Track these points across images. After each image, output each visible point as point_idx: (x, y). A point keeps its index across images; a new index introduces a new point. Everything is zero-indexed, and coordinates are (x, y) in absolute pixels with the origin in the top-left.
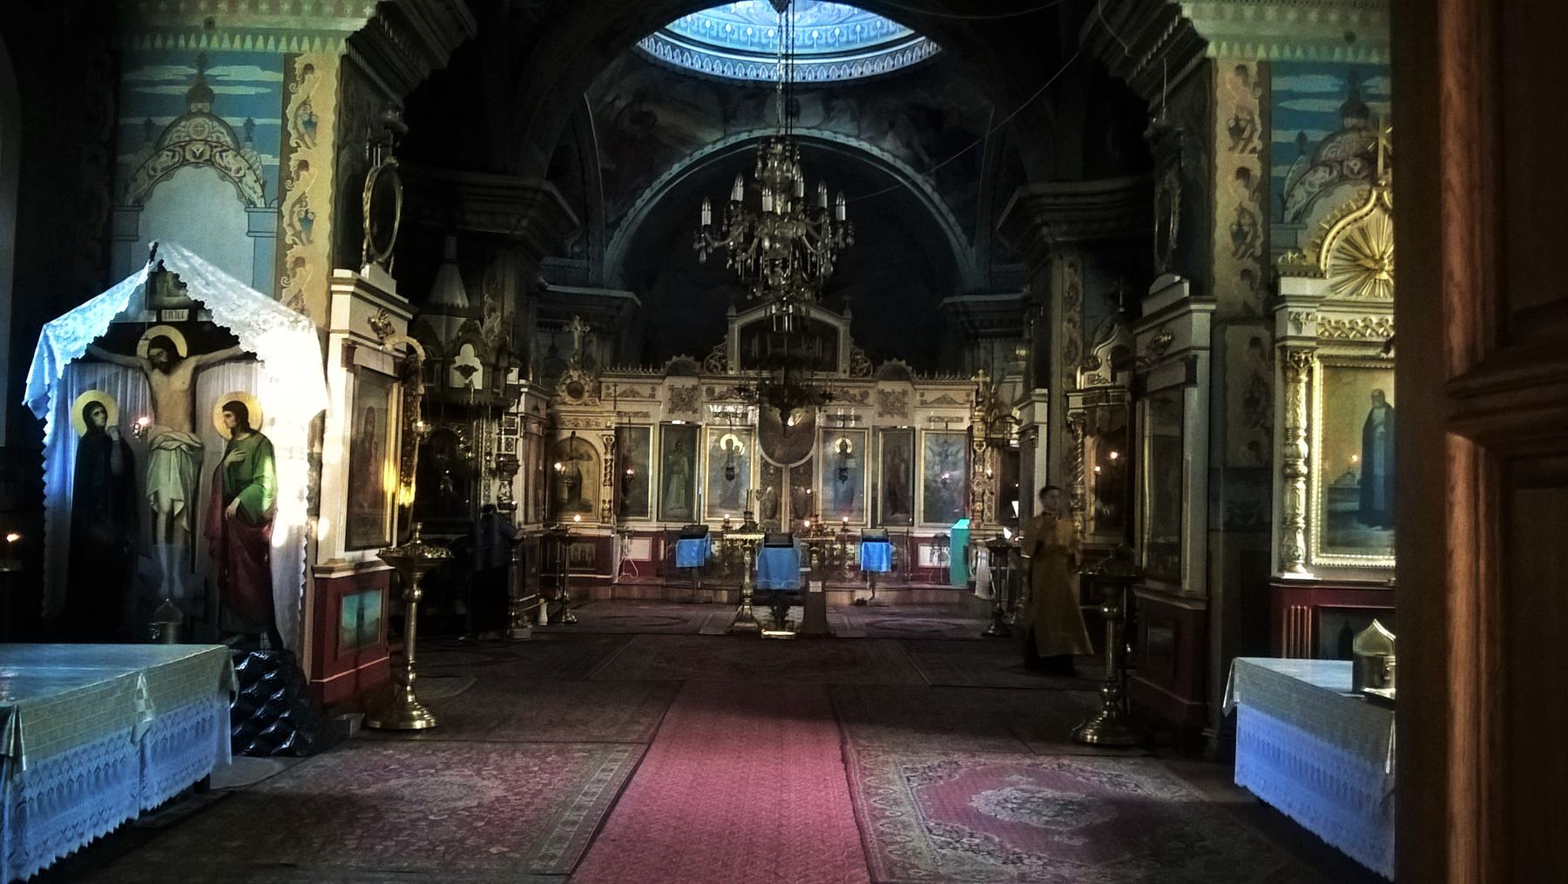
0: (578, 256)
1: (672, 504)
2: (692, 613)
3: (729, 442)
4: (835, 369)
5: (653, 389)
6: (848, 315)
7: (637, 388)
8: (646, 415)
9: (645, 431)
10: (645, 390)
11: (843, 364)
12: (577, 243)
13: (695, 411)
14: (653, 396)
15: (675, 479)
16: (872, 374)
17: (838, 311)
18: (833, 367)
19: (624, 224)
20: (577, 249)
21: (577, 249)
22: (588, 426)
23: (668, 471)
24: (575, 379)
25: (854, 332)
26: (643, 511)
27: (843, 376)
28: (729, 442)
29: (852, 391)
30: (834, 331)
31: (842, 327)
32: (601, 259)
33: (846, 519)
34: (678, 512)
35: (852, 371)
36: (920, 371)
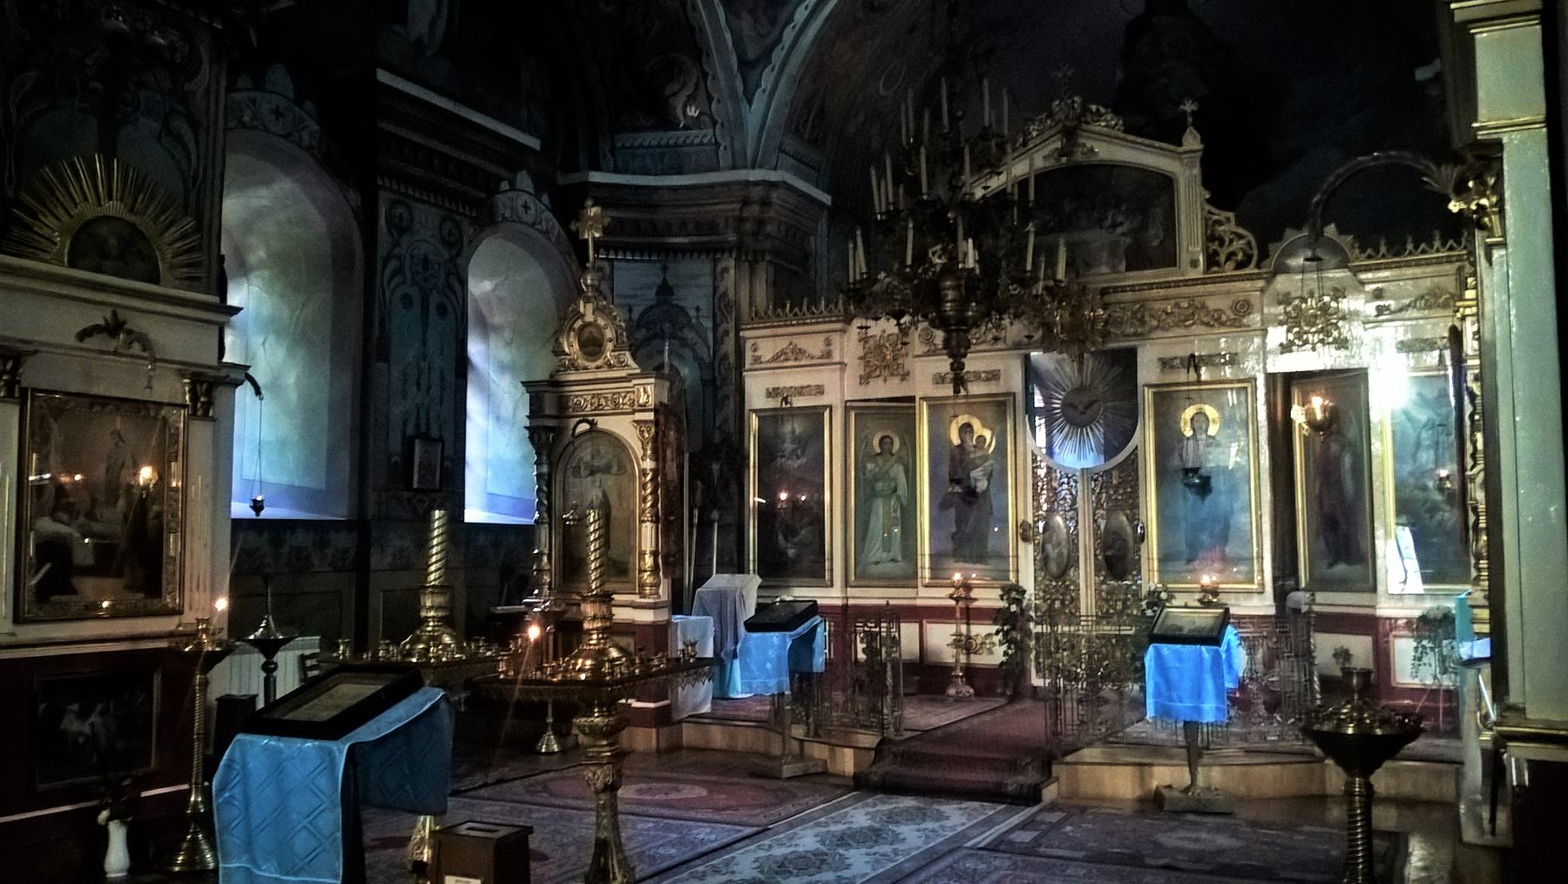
0: (696, 123)
1: (876, 552)
2: (1033, 671)
3: (966, 429)
4: (1170, 260)
5: (828, 343)
6: (1192, 141)
7: (802, 343)
8: (820, 390)
9: (815, 416)
10: (814, 345)
11: (1191, 245)
12: (691, 100)
13: (905, 376)
14: (829, 354)
15: (879, 506)
16: (1263, 256)
17: (1170, 134)
18: (1168, 258)
19: (778, 56)
20: (692, 112)
21: (692, 112)
22: (617, 411)
23: (867, 490)
24: (589, 318)
25: (1209, 179)
26: (816, 572)
27: (1198, 273)
28: (966, 429)
29: (1212, 304)
30: (1165, 184)
31: (1181, 163)
32: (738, 125)
33: (1206, 580)
34: (889, 568)
35: (1212, 260)
36: (1367, 243)
